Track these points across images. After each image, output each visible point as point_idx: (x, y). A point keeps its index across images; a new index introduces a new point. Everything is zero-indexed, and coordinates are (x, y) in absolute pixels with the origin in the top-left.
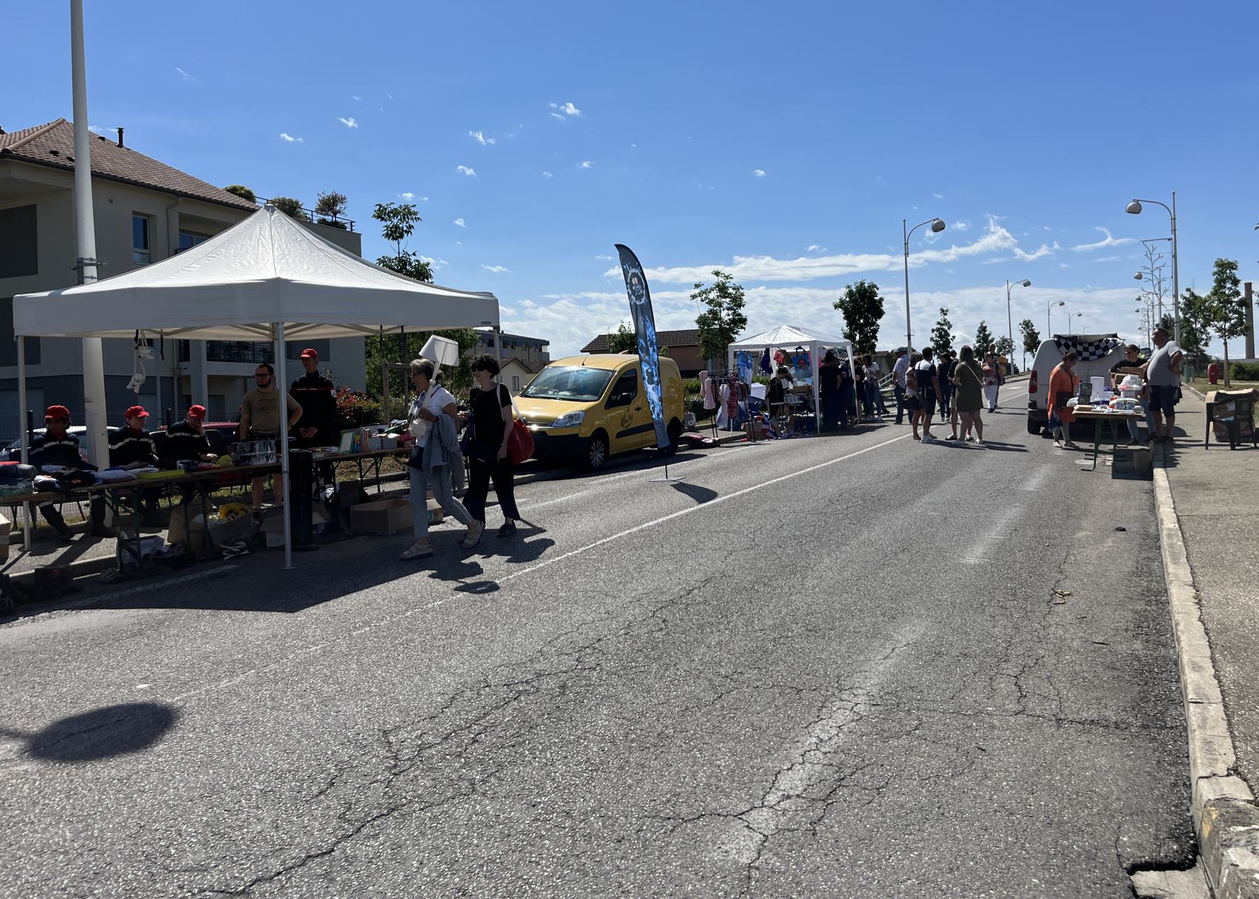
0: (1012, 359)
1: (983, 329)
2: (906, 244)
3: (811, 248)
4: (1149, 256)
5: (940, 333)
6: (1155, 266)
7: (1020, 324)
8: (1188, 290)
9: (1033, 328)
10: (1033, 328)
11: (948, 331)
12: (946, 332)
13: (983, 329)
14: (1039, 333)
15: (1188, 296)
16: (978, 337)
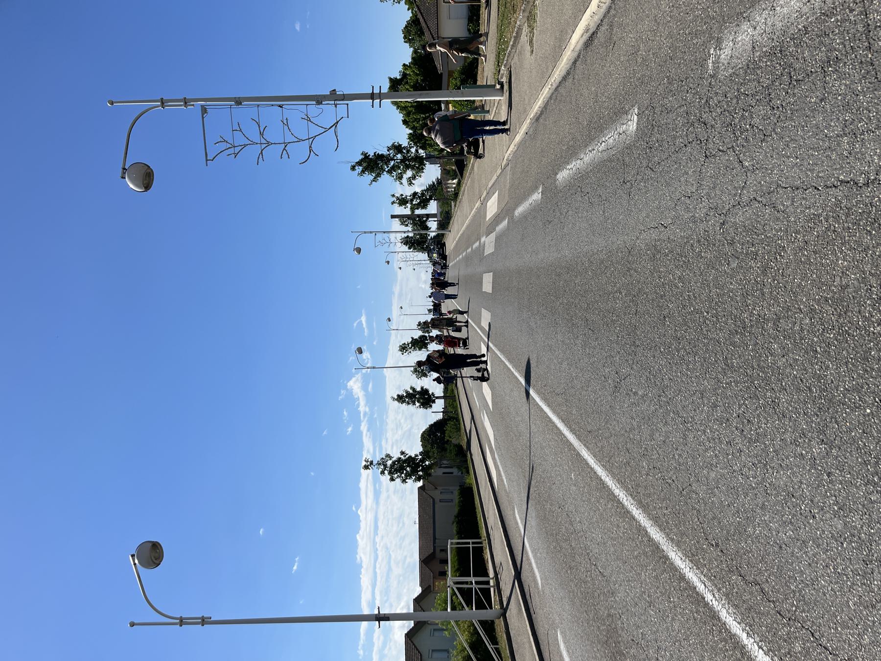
0: (372, 175)
1: (400, 399)
2: (182, 622)
3: (354, 509)
4: (237, 149)
5: (397, 471)
6: (256, 138)
7: (403, 354)
8: (353, 168)
9: (406, 343)
10: (406, 343)
11: (394, 459)
12: (394, 463)
13: (400, 399)
14: (412, 338)
15: (361, 168)
16: (408, 403)
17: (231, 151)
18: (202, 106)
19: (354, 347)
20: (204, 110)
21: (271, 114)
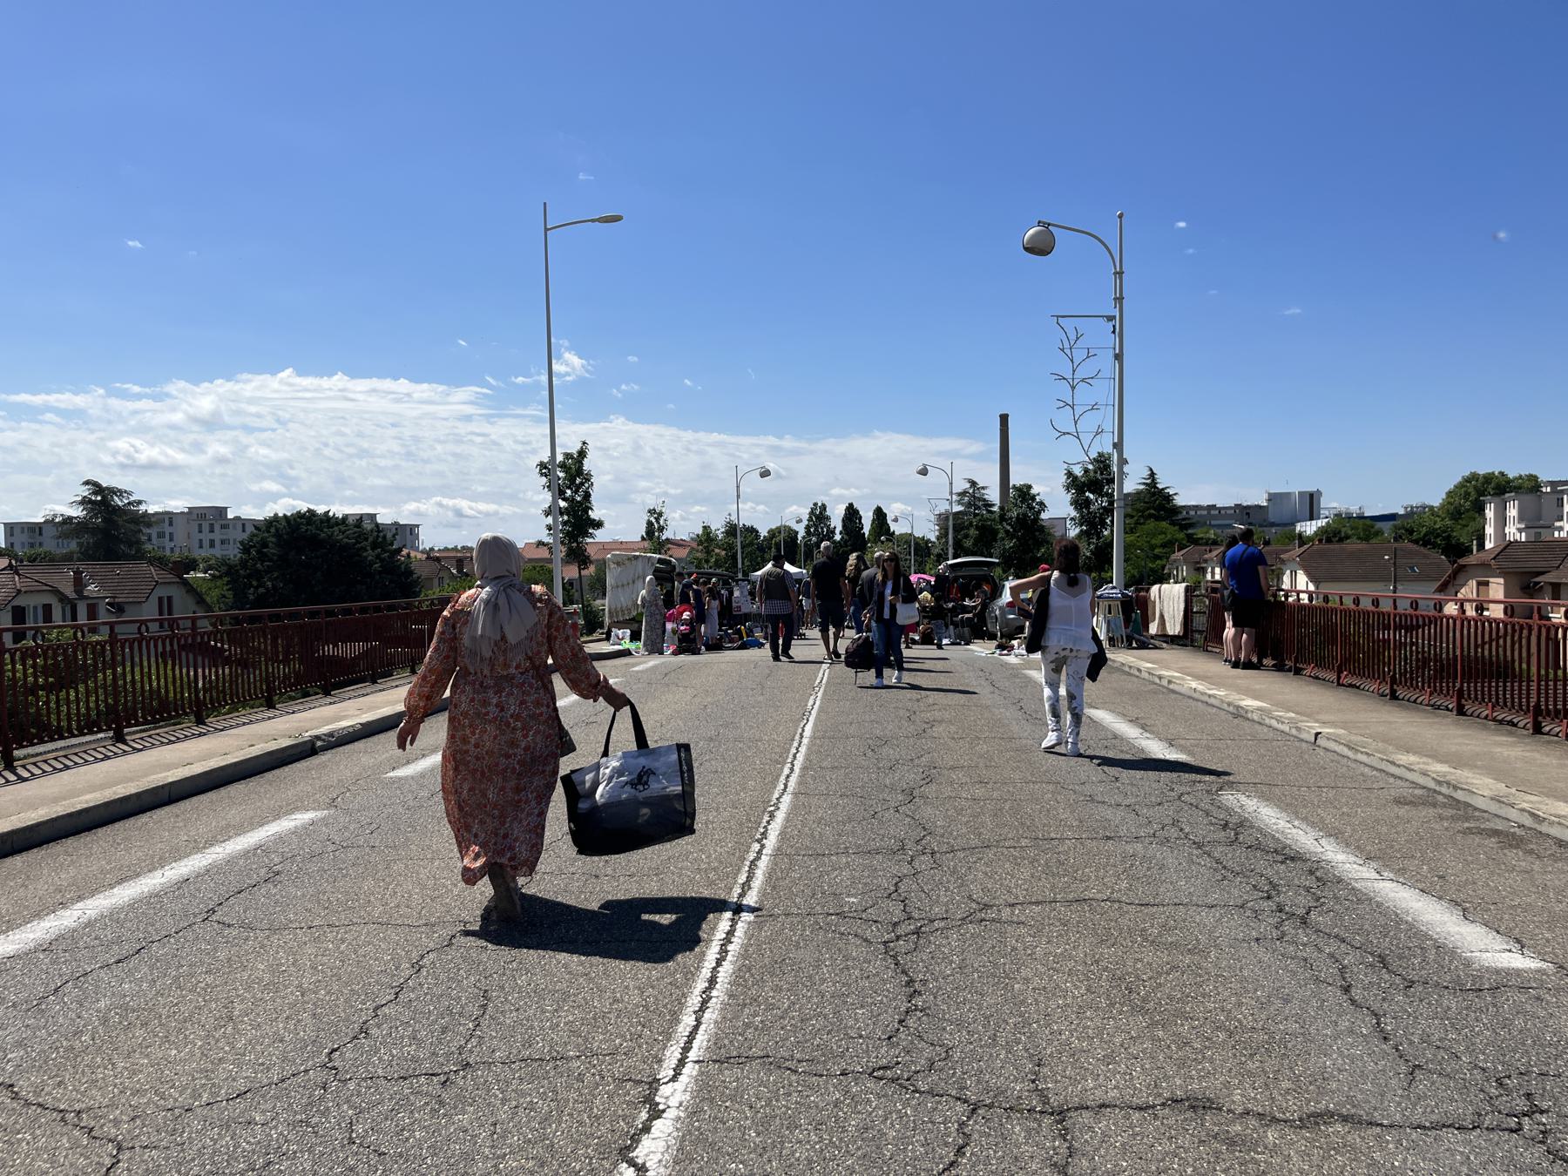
4: (1068, 352)
6: (1079, 375)
17: (1067, 345)
18: (1114, 317)
19: (771, 466)
20: (1111, 318)
21: (1103, 392)
